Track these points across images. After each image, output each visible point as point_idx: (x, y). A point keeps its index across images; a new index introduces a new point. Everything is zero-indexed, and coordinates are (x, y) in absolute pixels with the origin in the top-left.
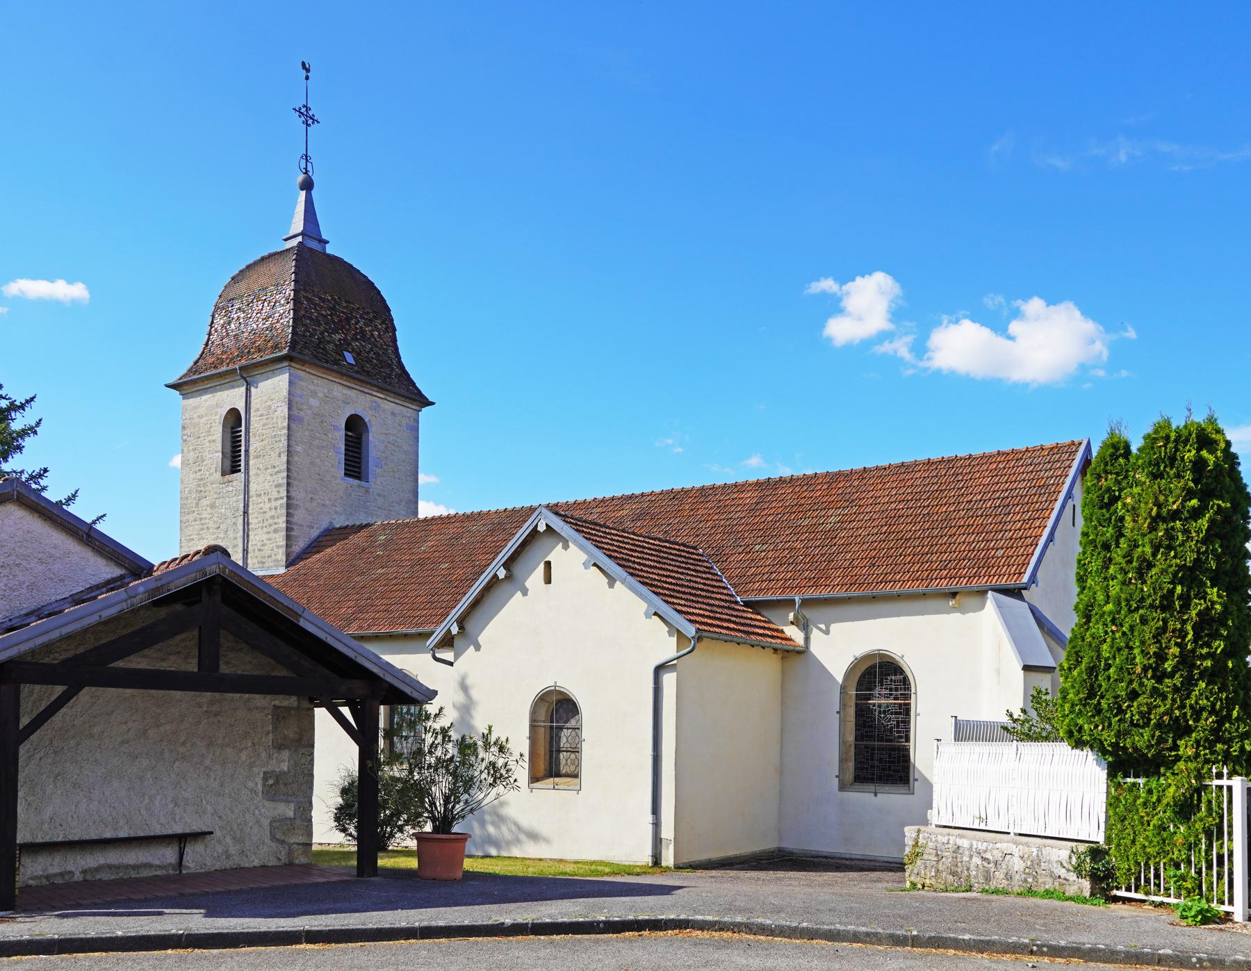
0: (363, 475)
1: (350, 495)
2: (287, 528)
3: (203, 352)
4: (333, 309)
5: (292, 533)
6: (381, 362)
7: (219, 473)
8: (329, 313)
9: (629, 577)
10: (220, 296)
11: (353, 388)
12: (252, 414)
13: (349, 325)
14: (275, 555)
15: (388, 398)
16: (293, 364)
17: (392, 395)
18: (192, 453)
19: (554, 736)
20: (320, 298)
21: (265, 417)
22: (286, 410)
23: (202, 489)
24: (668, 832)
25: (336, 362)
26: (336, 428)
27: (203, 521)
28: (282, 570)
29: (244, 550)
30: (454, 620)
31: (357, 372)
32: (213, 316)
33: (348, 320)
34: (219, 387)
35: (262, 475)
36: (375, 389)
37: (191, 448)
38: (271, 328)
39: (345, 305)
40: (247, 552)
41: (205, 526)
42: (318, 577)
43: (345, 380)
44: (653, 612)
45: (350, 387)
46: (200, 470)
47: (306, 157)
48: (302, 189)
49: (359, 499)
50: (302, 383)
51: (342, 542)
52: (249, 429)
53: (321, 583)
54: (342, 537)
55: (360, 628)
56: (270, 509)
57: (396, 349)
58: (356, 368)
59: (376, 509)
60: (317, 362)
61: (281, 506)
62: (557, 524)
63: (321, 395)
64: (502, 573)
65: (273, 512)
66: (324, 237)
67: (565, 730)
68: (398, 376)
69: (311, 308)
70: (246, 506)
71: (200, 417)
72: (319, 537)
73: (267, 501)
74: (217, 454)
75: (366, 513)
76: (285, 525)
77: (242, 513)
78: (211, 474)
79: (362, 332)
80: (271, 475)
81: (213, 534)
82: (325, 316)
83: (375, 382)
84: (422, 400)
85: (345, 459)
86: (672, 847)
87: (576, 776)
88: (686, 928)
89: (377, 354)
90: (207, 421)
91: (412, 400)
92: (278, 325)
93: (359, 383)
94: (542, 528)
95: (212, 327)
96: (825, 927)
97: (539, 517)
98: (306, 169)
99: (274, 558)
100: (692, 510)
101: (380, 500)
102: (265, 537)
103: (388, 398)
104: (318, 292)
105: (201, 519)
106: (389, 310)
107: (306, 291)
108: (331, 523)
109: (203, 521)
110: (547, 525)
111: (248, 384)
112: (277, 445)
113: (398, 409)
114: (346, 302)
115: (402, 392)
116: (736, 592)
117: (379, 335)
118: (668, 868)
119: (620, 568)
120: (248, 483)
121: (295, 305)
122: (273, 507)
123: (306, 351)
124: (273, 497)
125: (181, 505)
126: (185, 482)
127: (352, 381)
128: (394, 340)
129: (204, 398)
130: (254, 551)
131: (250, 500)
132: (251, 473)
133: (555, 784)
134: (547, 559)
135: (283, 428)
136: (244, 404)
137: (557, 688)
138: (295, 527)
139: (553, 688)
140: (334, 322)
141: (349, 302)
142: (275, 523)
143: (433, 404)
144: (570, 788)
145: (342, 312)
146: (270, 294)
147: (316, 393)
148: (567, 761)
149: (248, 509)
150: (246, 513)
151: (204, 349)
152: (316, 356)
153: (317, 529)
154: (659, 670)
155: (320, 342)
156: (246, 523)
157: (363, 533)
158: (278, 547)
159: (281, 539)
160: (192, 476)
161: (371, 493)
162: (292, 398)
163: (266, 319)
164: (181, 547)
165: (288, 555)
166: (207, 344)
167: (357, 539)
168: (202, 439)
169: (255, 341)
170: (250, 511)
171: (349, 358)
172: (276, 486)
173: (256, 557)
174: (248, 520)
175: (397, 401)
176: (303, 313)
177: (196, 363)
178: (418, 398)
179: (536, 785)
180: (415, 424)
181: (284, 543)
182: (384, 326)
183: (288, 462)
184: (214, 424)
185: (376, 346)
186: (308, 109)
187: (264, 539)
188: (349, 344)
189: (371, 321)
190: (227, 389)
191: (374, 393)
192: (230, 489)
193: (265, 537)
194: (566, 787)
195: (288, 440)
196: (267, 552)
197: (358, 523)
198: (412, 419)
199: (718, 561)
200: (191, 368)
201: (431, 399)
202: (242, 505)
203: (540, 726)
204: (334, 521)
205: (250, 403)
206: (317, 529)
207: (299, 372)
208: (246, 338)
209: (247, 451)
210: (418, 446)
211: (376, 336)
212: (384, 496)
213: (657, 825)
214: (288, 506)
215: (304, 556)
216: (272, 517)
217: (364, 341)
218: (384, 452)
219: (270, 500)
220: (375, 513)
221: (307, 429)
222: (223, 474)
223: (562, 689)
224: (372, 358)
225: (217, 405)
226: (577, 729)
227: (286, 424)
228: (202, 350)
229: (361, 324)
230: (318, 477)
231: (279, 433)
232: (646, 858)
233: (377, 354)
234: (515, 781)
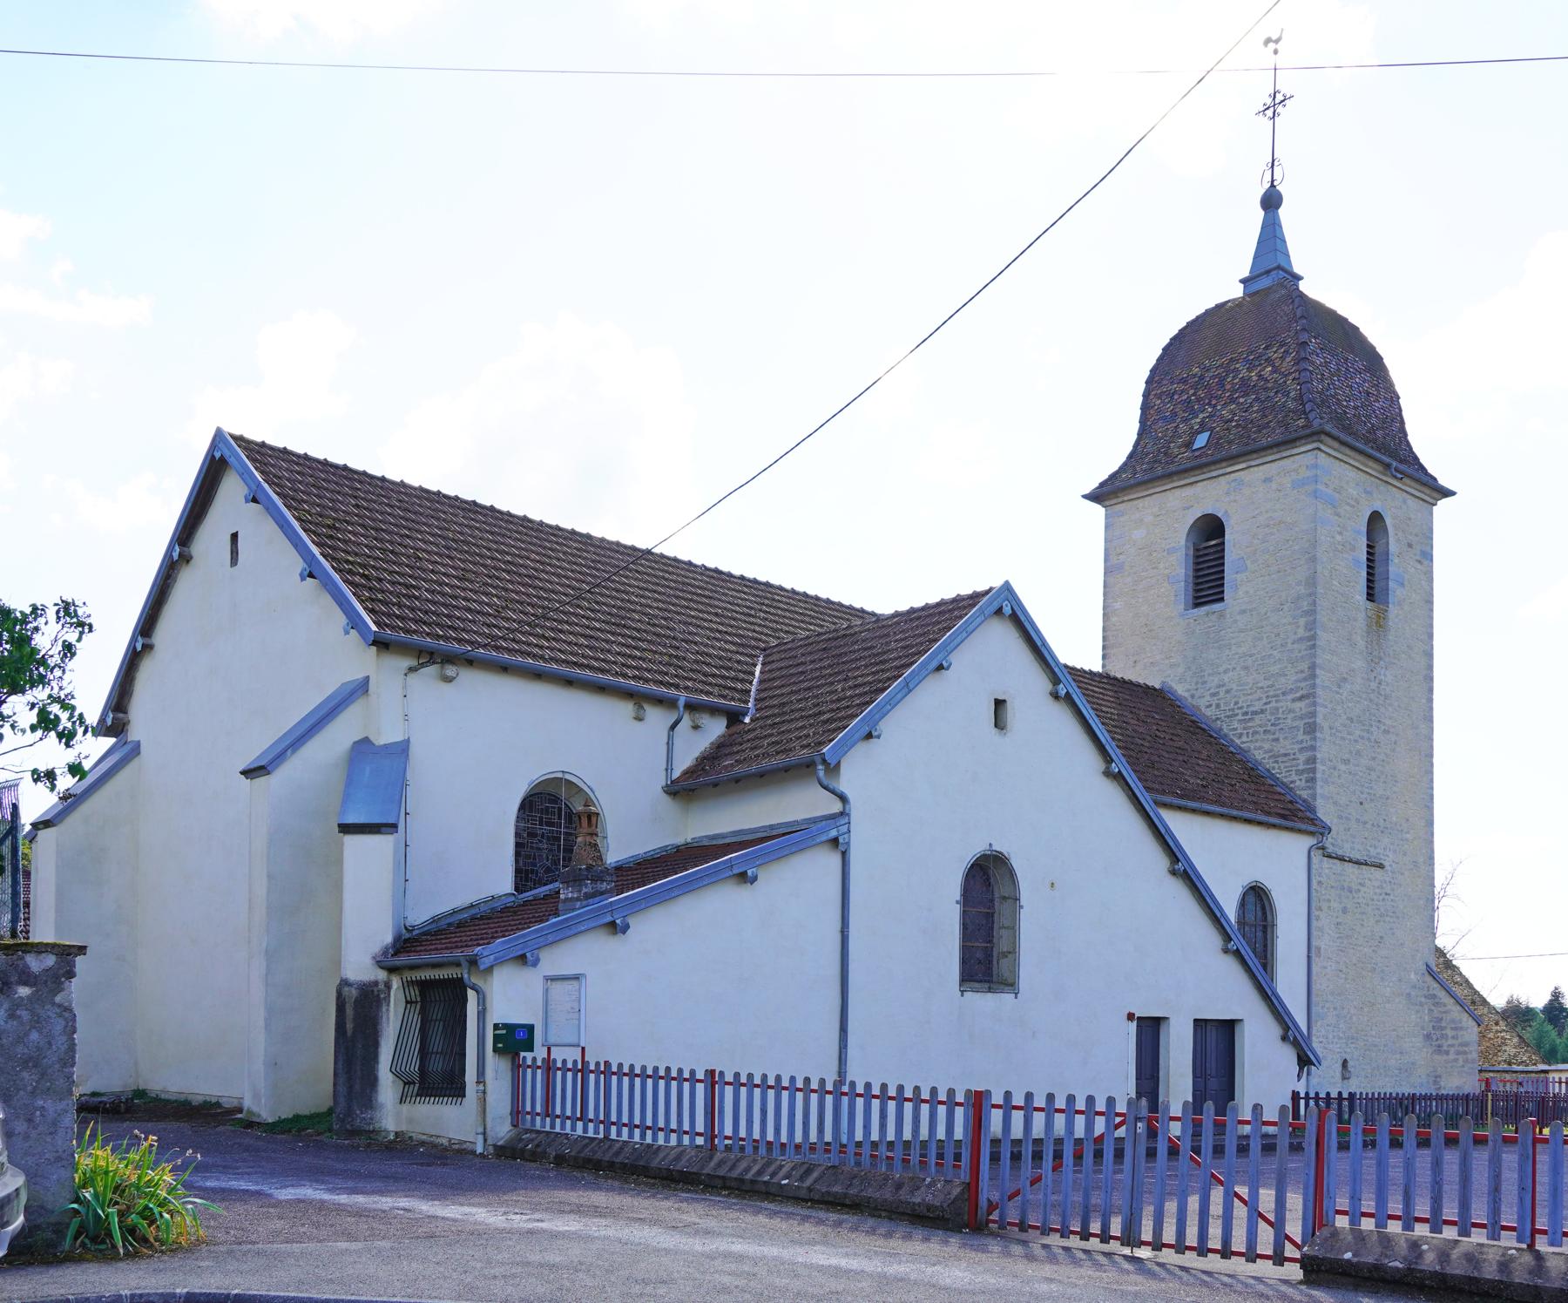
11: (1197, 482)
15: (1253, 463)
17: (1255, 456)
36: (1224, 464)
93: (1197, 472)
143: (1452, 493)
191: (1229, 470)
201: (1443, 481)
204: (1168, 680)
220: (1233, 641)
223: (1262, 886)
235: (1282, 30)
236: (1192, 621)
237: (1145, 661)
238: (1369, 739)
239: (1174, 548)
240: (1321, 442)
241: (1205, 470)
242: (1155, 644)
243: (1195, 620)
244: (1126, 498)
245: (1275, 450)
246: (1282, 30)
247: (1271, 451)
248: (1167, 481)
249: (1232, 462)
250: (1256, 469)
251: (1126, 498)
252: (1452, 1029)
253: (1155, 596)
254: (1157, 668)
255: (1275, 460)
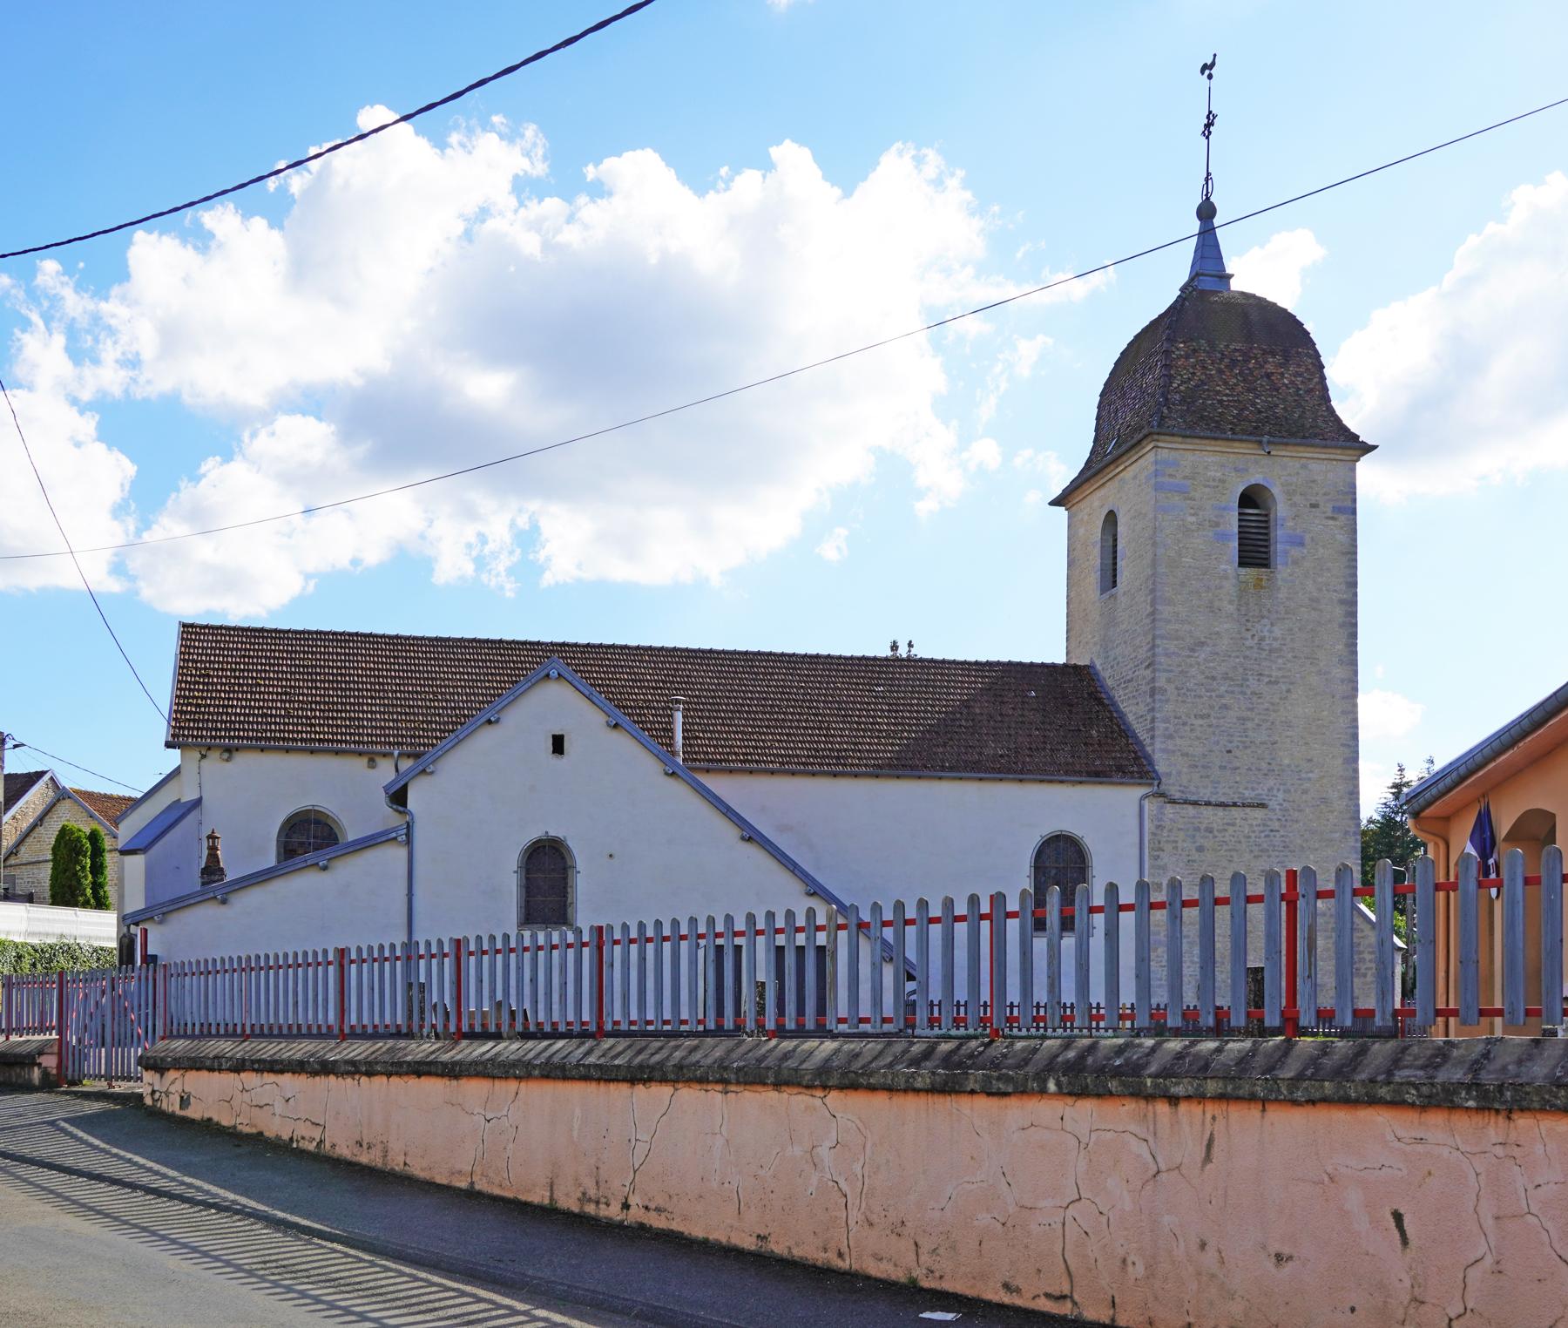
15: (1127, 464)
143: (1375, 447)
235: (1215, 55)
238: (1243, 693)
240: (1158, 441)
246: (1215, 55)
252: (1369, 953)
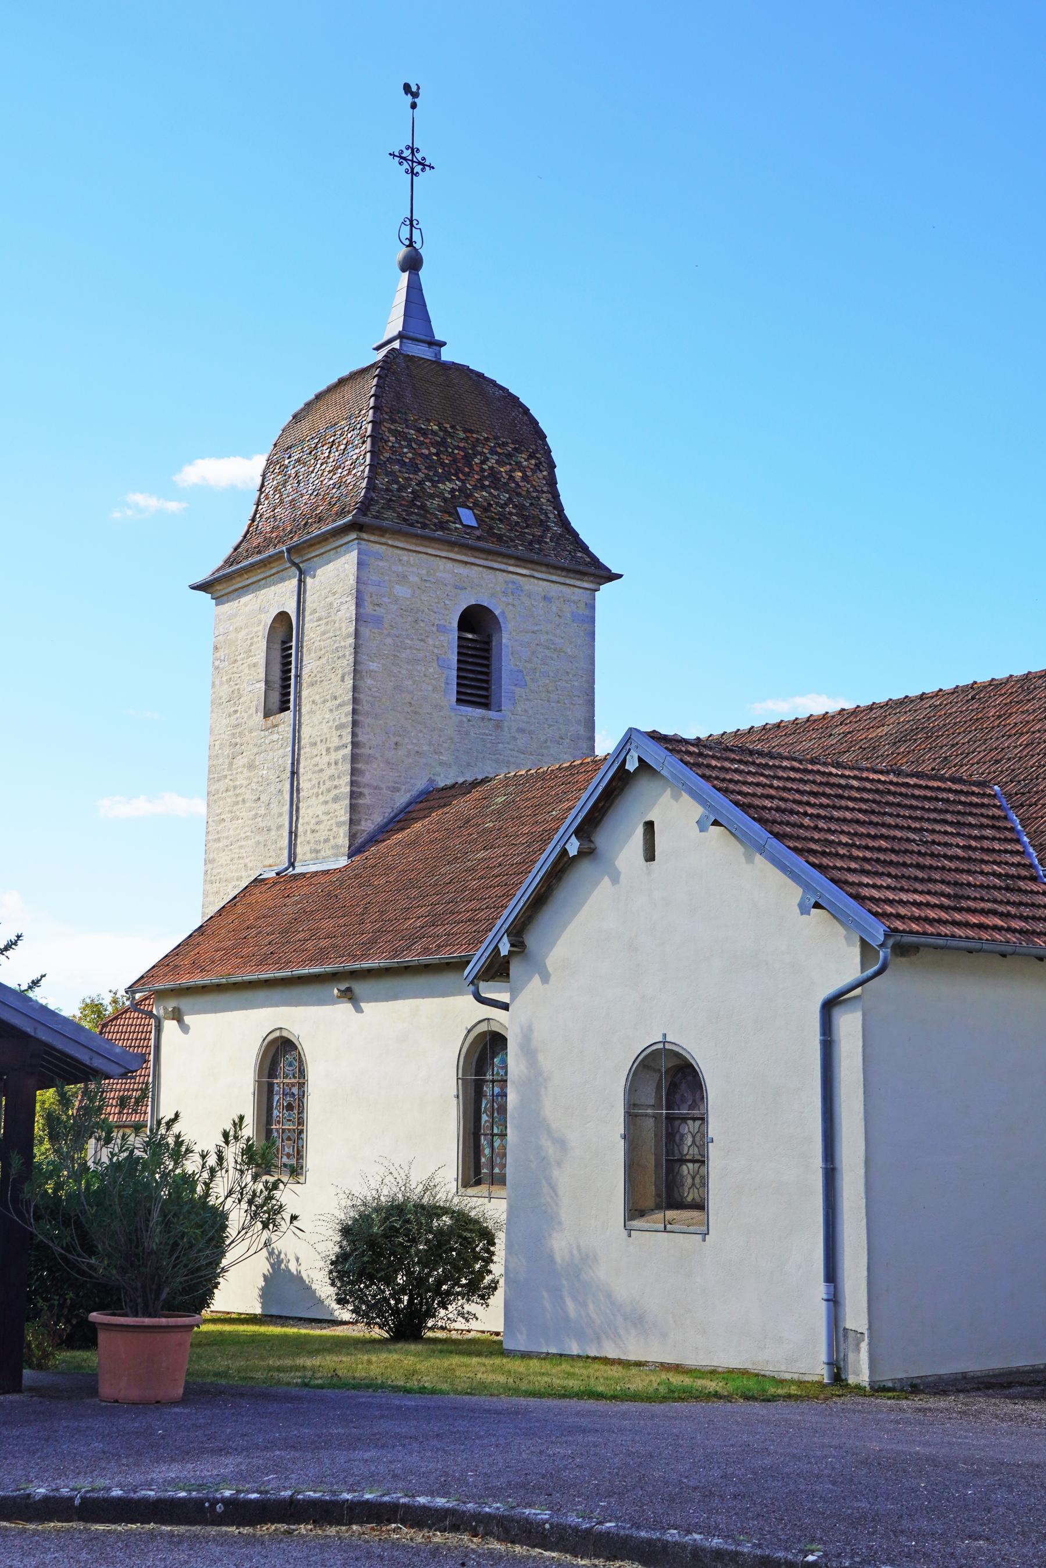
0: (494, 699)
1: (467, 733)
2: (352, 793)
3: (247, 532)
4: (443, 443)
5: (360, 801)
6: (526, 518)
7: (261, 714)
8: (434, 450)
9: (774, 842)
10: (275, 445)
12: (307, 619)
13: (470, 466)
14: (334, 838)
15: (536, 574)
16: (365, 536)
17: (544, 569)
18: (226, 686)
19: (671, 1135)
20: (419, 430)
21: (324, 621)
22: (354, 607)
23: (238, 740)
24: (856, 1318)
25: (442, 526)
26: (442, 629)
27: (238, 791)
28: (343, 862)
29: (291, 833)
30: (503, 930)
31: (479, 538)
32: (264, 476)
33: (468, 459)
34: (263, 582)
35: (318, 713)
36: (512, 562)
37: (224, 679)
38: (338, 485)
39: (462, 435)
40: (296, 836)
41: (240, 799)
42: (390, 868)
43: (458, 553)
44: (813, 901)
45: (466, 563)
46: (236, 712)
47: (411, 221)
48: (403, 271)
49: (483, 740)
50: (381, 564)
51: (440, 812)
52: (302, 642)
53: (391, 879)
54: (442, 802)
55: (426, 950)
56: (329, 764)
57: (556, 495)
58: (478, 533)
59: (515, 753)
60: (406, 528)
61: (344, 757)
62: (656, 756)
63: (414, 579)
64: (573, 847)
65: (332, 770)
66: (438, 336)
67: (690, 1122)
68: (557, 539)
69: (402, 447)
70: (295, 763)
71: (238, 630)
72: (409, 804)
73: (324, 752)
74: (258, 685)
75: (497, 761)
76: (348, 789)
77: (289, 775)
78: (250, 717)
79: (494, 475)
80: (331, 710)
81: (251, 809)
82: (427, 457)
83: (511, 551)
84: (598, 572)
85: (458, 677)
86: (864, 1346)
87: (700, 1206)
88: (390, 1522)
89: (520, 507)
90: (247, 634)
91: (581, 574)
92: (349, 479)
93: (482, 555)
94: (631, 766)
95: (261, 493)
96: (643, 1534)
97: (628, 747)
98: (411, 239)
99: (332, 842)
100: (999, 717)
101: (522, 740)
102: (320, 810)
103: (536, 574)
104: (416, 421)
105: (235, 788)
106: (543, 437)
107: (393, 421)
108: (431, 781)
109: (238, 791)
110: (640, 759)
111: (301, 572)
112: (339, 662)
113: (554, 590)
114: (465, 431)
115: (565, 563)
116: (1040, 860)
117: (525, 478)
118: (858, 1387)
119: (757, 826)
120: (300, 726)
121: (373, 444)
122: (333, 761)
123: (388, 514)
124: (332, 746)
125: (210, 767)
126: (216, 732)
127: (469, 553)
128: (552, 482)
129: (244, 600)
130: (305, 833)
131: (302, 752)
132: (304, 710)
133: (667, 1223)
134: (648, 819)
135: (348, 636)
136: (294, 604)
137: (667, 1046)
138: (366, 791)
139: (661, 1046)
140: (443, 465)
141: (471, 431)
142: (336, 787)
143: (620, 576)
144: (692, 1229)
145: (458, 448)
146: (339, 433)
147: (405, 577)
148: (693, 1178)
149: (298, 768)
150: (294, 773)
151: (250, 526)
152: (405, 520)
153: (406, 792)
154: (830, 1006)
155: (415, 498)
156: (295, 790)
157: (476, 794)
158: (339, 824)
159: (343, 811)
160: (225, 722)
161: (506, 729)
162: (362, 587)
163: (333, 471)
164: (207, 833)
165: (352, 836)
166: (253, 520)
167: (462, 805)
168: (240, 663)
169: (318, 506)
170: (301, 771)
171: (467, 517)
172: (338, 728)
173: (308, 843)
174: (298, 784)
175: (554, 578)
176: (387, 455)
177: (236, 549)
178: (592, 570)
179: (636, 1223)
180: (587, 612)
181: (345, 818)
182: (533, 462)
183: (355, 688)
184: (255, 640)
185: (519, 495)
186: (413, 150)
187: (320, 813)
188: (469, 496)
189: (509, 456)
190: (274, 584)
191: (511, 569)
192: (275, 737)
193: (320, 810)
194: (685, 1228)
195: (356, 653)
196: (322, 835)
197: (470, 779)
198: (582, 605)
199: (1022, 805)
200: (229, 558)
202: (290, 762)
203: (646, 1115)
205: (304, 602)
206: (406, 792)
207: (378, 546)
208: (306, 504)
209: (298, 676)
210: (594, 646)
211: (518, 479)
212: (531, 733)
213: (834, 1301)
214: (354, 758)
215: (380, 837)
216: (332, 777)
217: (496, 489)
218: (530, 661)
219: (328, 750)
220: (512, 760)
221: (389, 635)
222: (266, 715)
224: (511, 513)
225: (261, 610)
226: (703, 1119)
227: (352, 629)
228: (246, 528)
229: (492, 462)
230: (408, 709)
231: (343, 644)
232: (818, 1370)
233: (520, 507)
234: (294, 1218)
236: (465, 719)
237: (409, 747)
239: (444, 626)
241: (490, 558)
242: (421, 731)
243: (469, 720)
244: (390, 542)
245: (564, 573)
247: (559, 572)
248: (447, 548)
249: (519, 563)
250: (536, 581)
251: (390, 542)
253: (422, 675)
254: (424, 760)
255: (557, 582)
